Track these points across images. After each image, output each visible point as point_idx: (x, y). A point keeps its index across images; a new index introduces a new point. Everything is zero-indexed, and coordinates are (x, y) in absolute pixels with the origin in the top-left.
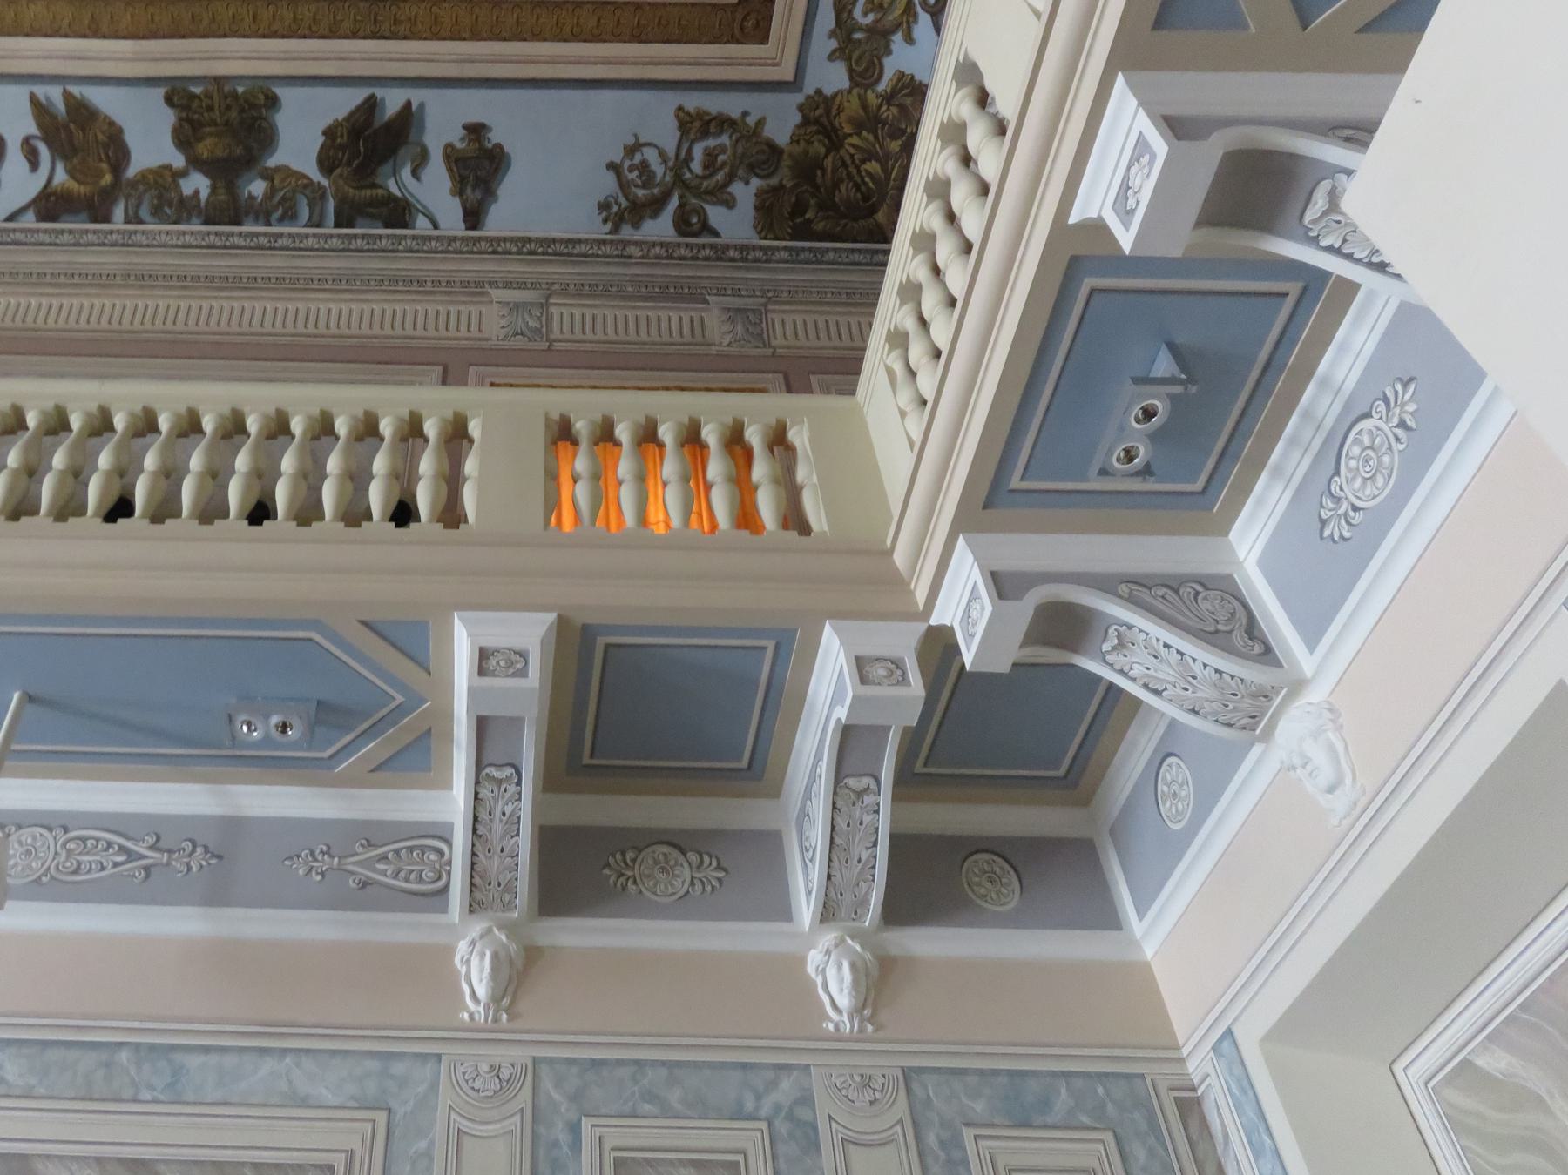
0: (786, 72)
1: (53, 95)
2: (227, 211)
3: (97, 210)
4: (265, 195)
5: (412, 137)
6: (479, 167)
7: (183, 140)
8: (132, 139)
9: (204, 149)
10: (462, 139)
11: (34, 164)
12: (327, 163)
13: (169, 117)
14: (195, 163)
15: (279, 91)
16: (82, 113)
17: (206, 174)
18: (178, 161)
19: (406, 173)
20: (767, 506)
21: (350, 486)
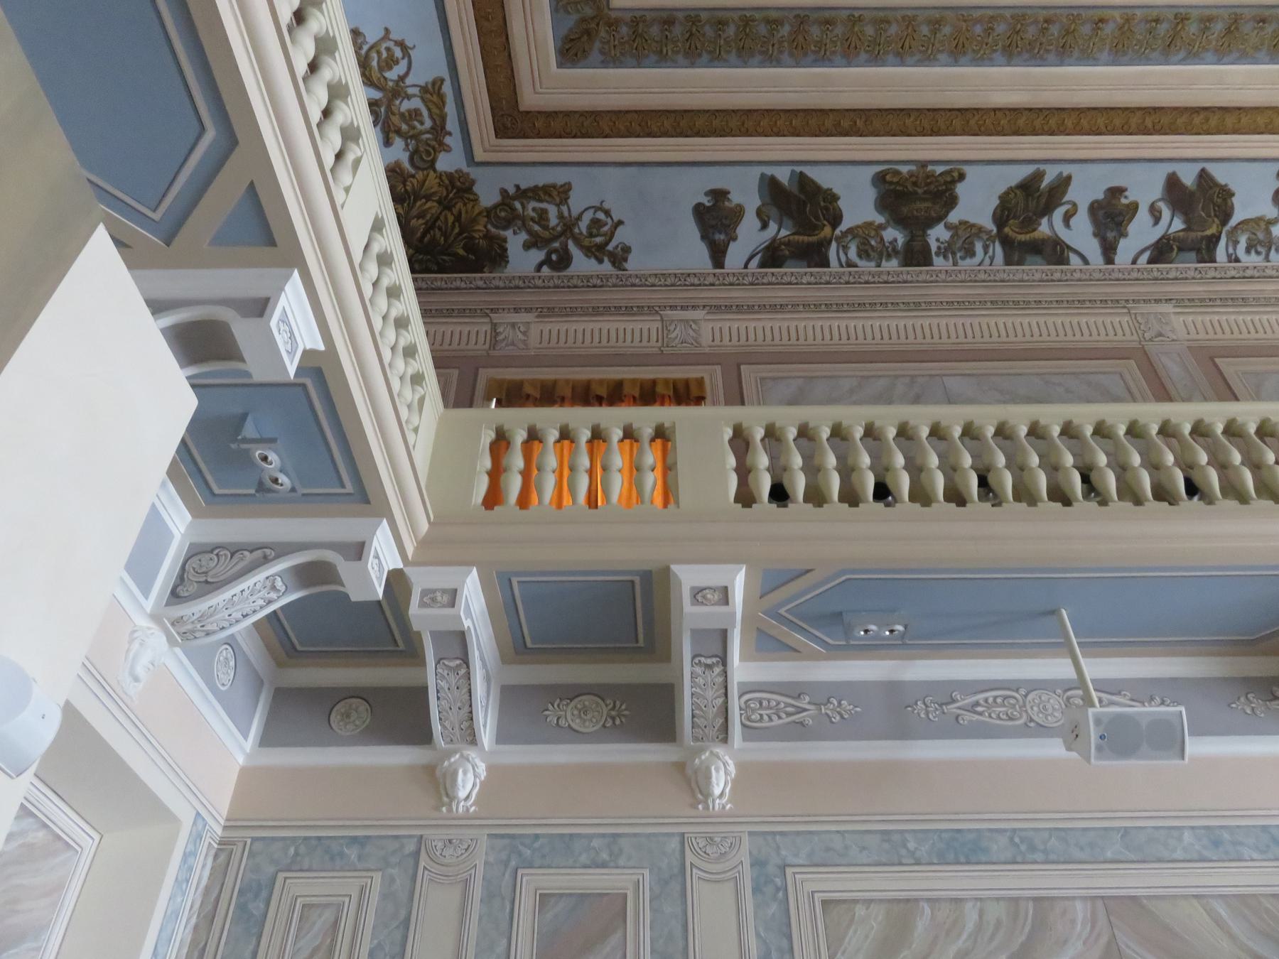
0: (479, 155)
1: (783, 175)
2: (916, 255)
3: (815, 255)
11: (1157, 220)
15: (967, 169)
20: (514, 485)
21: (918, 461)
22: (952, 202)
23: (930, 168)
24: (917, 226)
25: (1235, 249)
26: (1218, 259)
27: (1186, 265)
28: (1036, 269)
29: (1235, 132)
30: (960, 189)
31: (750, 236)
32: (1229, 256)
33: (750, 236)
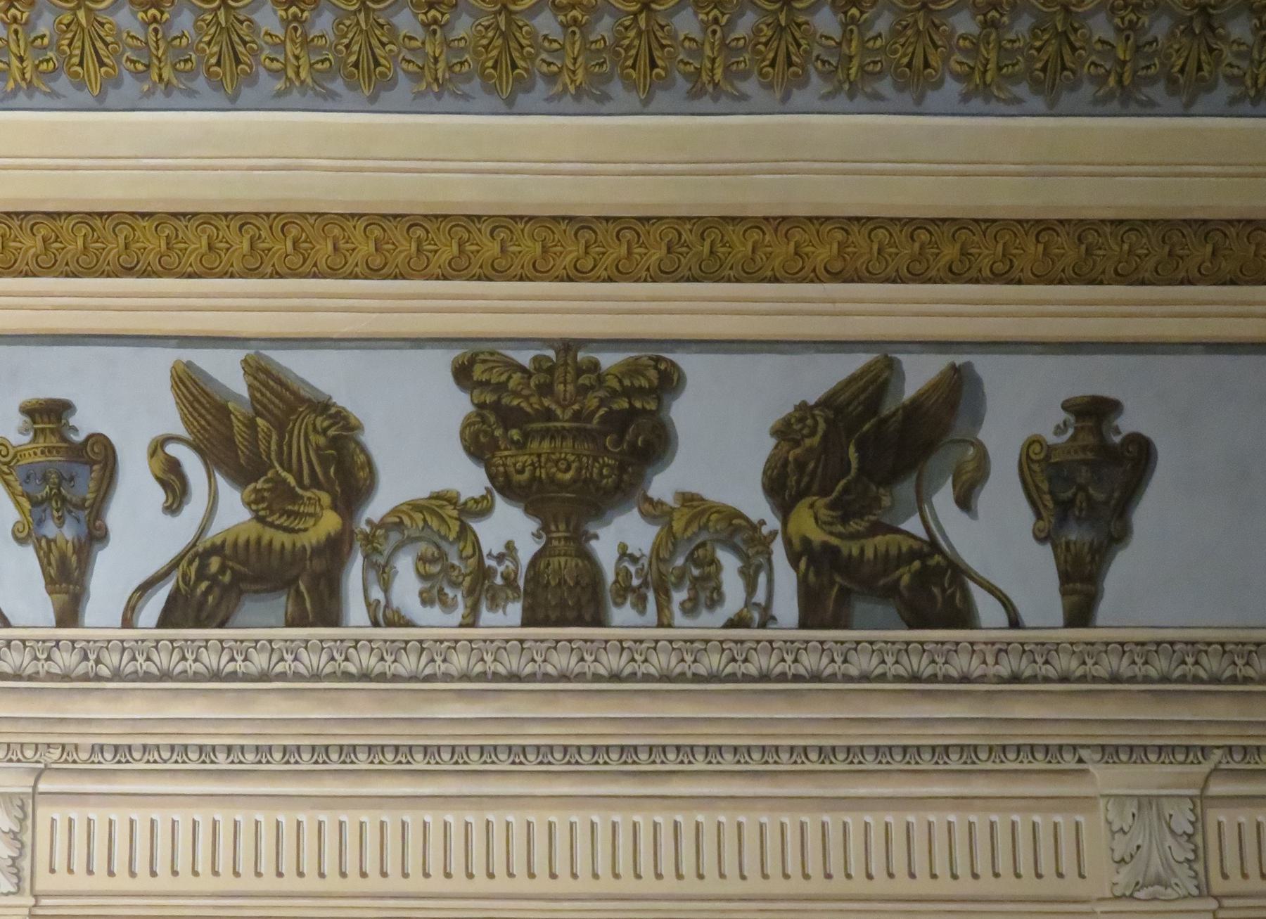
1: (227, 372)
4: (656, 549)
5: (960, 427)
6: (1093, 482)
7: (478, 445)
8: (377, 440)
9: (518, 462)
10: (1059, 430)
12: (782, 486)
13: (461, 405)
14: (505, 486)
15: (684, 360)
16: (281, 399)
17: (532, 509)
18: (470, 480)
19: (943, 499)
22: (654, 445)
23: (581, 355)
24: (568, 508)
25: (386, 589)
26: (353, 622)
27: (262, 631)
28: (877, 638)
29: (333, 273)
30: (682, 413)
31: (142, 535)
32: (371, 606)
33: (142, 535)
